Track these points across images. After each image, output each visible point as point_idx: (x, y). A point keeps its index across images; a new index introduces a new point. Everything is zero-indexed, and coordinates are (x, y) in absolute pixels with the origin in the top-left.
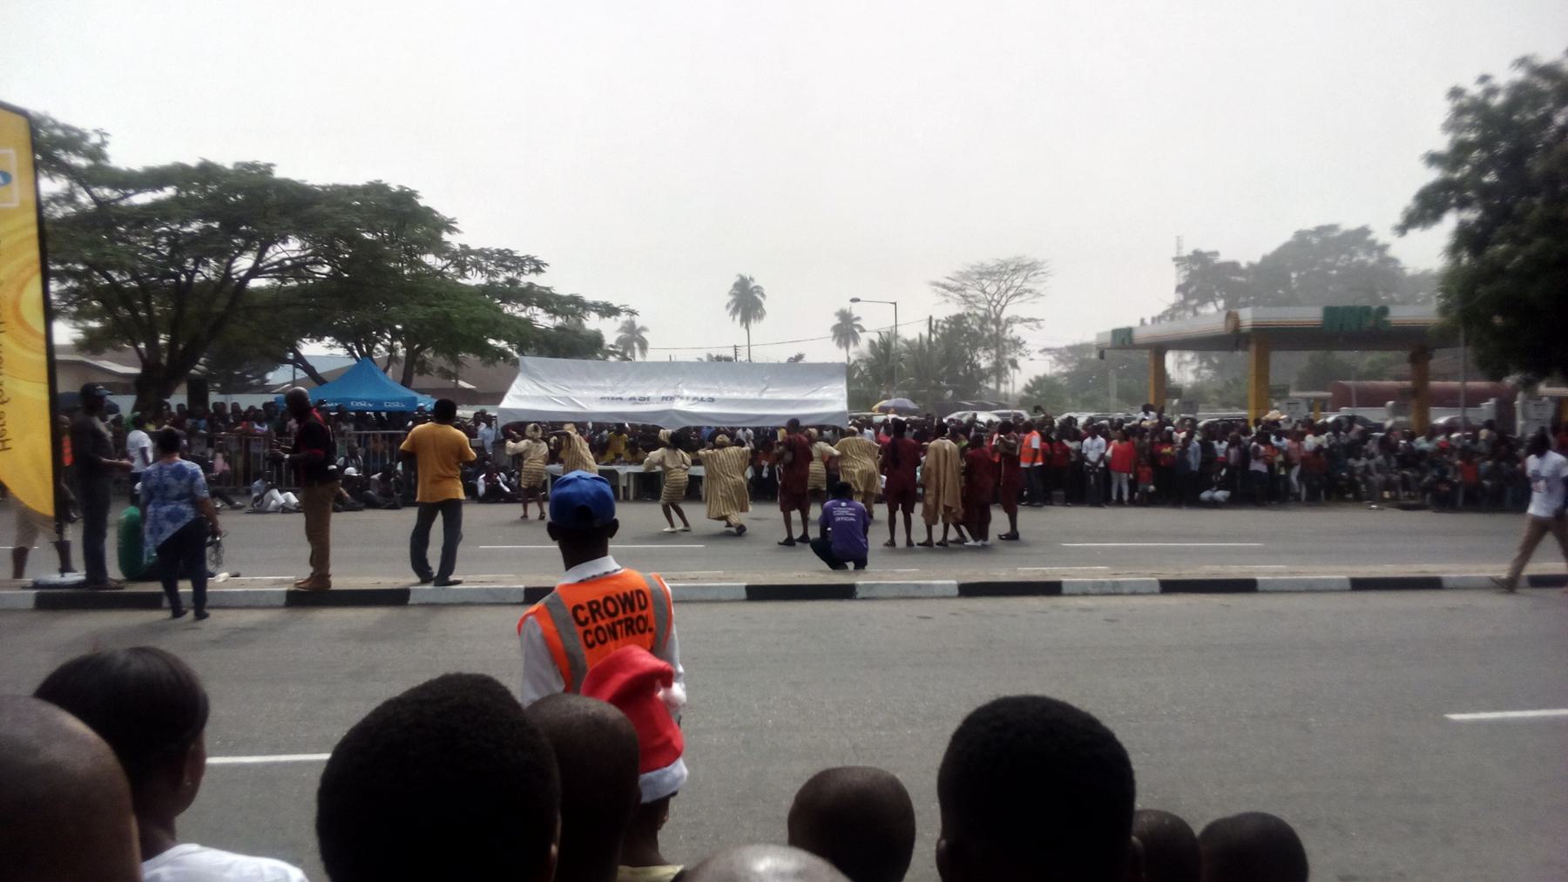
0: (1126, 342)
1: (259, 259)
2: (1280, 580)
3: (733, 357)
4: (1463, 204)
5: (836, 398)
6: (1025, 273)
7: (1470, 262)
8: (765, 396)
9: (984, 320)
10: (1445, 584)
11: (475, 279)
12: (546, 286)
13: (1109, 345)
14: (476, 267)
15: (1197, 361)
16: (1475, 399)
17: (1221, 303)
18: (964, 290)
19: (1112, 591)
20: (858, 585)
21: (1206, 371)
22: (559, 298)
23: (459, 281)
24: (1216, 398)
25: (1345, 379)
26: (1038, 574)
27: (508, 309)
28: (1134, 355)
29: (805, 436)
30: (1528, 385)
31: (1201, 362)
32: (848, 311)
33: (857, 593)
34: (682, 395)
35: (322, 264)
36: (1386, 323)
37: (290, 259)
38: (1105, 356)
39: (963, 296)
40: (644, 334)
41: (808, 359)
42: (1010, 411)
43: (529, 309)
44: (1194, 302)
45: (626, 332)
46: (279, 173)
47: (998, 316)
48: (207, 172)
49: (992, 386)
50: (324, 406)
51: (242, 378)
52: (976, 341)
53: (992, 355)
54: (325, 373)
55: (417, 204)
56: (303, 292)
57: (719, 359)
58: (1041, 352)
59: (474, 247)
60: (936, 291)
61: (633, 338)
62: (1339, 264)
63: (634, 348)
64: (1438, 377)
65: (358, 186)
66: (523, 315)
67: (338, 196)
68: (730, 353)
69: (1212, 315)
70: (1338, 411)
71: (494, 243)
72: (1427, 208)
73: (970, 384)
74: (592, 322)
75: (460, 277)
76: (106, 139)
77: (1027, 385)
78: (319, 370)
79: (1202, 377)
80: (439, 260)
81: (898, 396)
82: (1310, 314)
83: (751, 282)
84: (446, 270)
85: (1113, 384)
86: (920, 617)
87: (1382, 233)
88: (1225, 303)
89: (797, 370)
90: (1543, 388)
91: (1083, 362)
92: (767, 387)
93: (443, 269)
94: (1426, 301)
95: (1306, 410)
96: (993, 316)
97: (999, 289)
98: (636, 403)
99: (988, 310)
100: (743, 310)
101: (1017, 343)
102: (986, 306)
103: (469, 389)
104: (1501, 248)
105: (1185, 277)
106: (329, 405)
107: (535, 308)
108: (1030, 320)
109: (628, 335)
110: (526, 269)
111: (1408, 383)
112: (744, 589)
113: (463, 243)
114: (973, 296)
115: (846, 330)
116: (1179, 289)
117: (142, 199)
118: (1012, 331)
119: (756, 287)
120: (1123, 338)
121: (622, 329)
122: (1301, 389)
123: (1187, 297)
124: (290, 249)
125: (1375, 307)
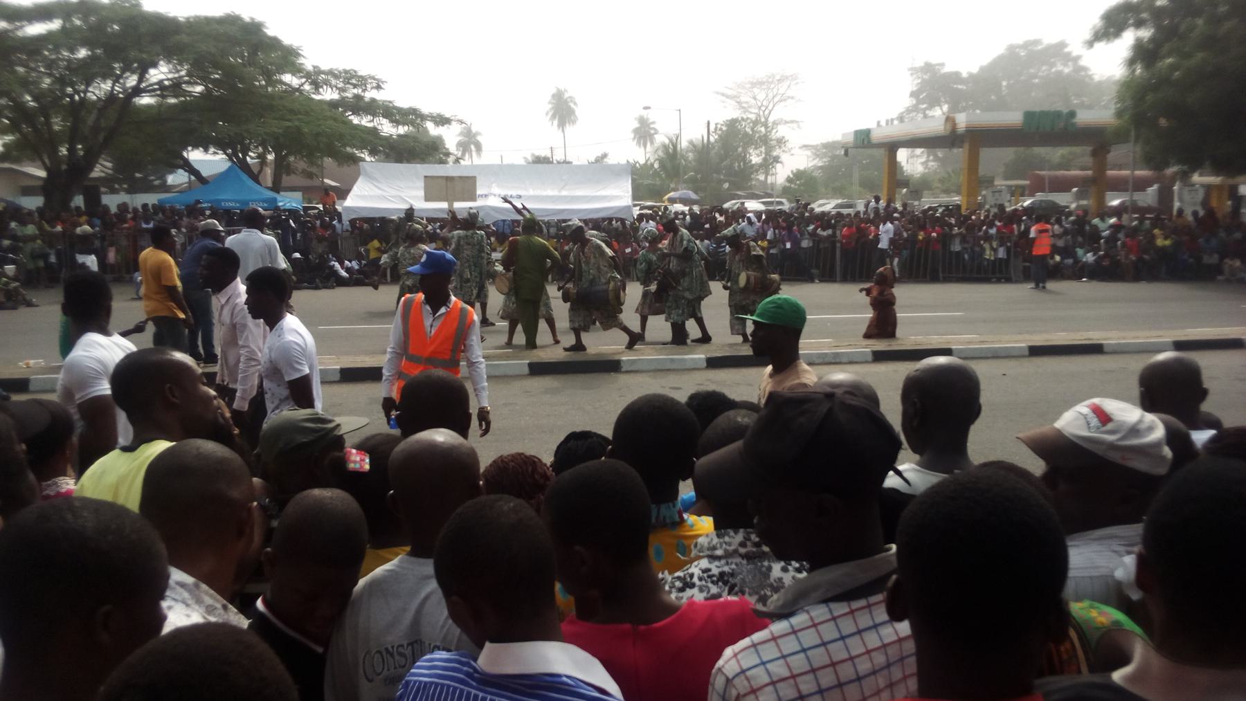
0: (866, 142)
1: (140, 80)
3: (550, 156)
4: (1139, 24)
5: (622, 194)
6: (788, 83)
7: (1141, 73)
8: (564, 193)
9: (756, 123)
10: (1106, 349)
11: (328, 95)
12: (389, 100)
13: (852, 145)
14: (326, 85)
16: (1141, 185)
17: (945, 108)
18: (739, 97)
19: (833, 361)
20: (622, 360)
21: (933, 164)
22: (400, 110)
23: (314, 96)
24: (939, 185)
25: (1040, 170)
27: (355, 120)
30: (1185, 176)
31: (928, 157)
32: (645, 117)
33: (622, 367)
35: (197, 84)
36: (1074, 124)
37: (168, 79)
39: (738, 102)
40: (479, 138)
41: (610, 160)
42: (773, 200)
44: (924, 106)
45: (465, 136)
47: (767, 120)
49: (762, 177)
50: (199, 206)
51: (144, 179)
53: (761, 152)
54: (208, 177)
55: (265, 34)
56: (183, 107)
58: (800, 148)
59: (324, 67)
62: (1040, 74)
63: (471, 151)
65: (216, 17)
69: (935, 120)
70: (1034, 196)
71: (340, 65)
72: (1112, 25)
73: (742, 179)
74: (432, 129)
75: (314, 93)
77: (789, 177)
78: (205, 173)
79: (929, 169)
81: (685, 189)
82: (1013, 118)
84: (302, 88)
85: (856, 177)
86: (671, 388)
87: (1076, 47)
88: (949, 108)
89: (600, 168)
90: (1196, 178)
91: (834, 157)
94: (1106, 107)
95: (1009, 195)
96: (763, 120)
101: (781, 142)
102: (756, 111)
104: (1169, 60)
105: (918, 84)
106: (203, 205)
107: (381, 118)
108: (792, 122)
111: (1090, 173)
112: (527, 365)
113: (315, 65)
114: (747, 103)
115: (644, 133)
116: (913, 94)
117: (36, 29)
119: (570, 97)
120: (863, 139)
121: (461, 134)
122: (1006, 179)
123: (919, 102)
124: (160, 73)
125: (1065, 111)
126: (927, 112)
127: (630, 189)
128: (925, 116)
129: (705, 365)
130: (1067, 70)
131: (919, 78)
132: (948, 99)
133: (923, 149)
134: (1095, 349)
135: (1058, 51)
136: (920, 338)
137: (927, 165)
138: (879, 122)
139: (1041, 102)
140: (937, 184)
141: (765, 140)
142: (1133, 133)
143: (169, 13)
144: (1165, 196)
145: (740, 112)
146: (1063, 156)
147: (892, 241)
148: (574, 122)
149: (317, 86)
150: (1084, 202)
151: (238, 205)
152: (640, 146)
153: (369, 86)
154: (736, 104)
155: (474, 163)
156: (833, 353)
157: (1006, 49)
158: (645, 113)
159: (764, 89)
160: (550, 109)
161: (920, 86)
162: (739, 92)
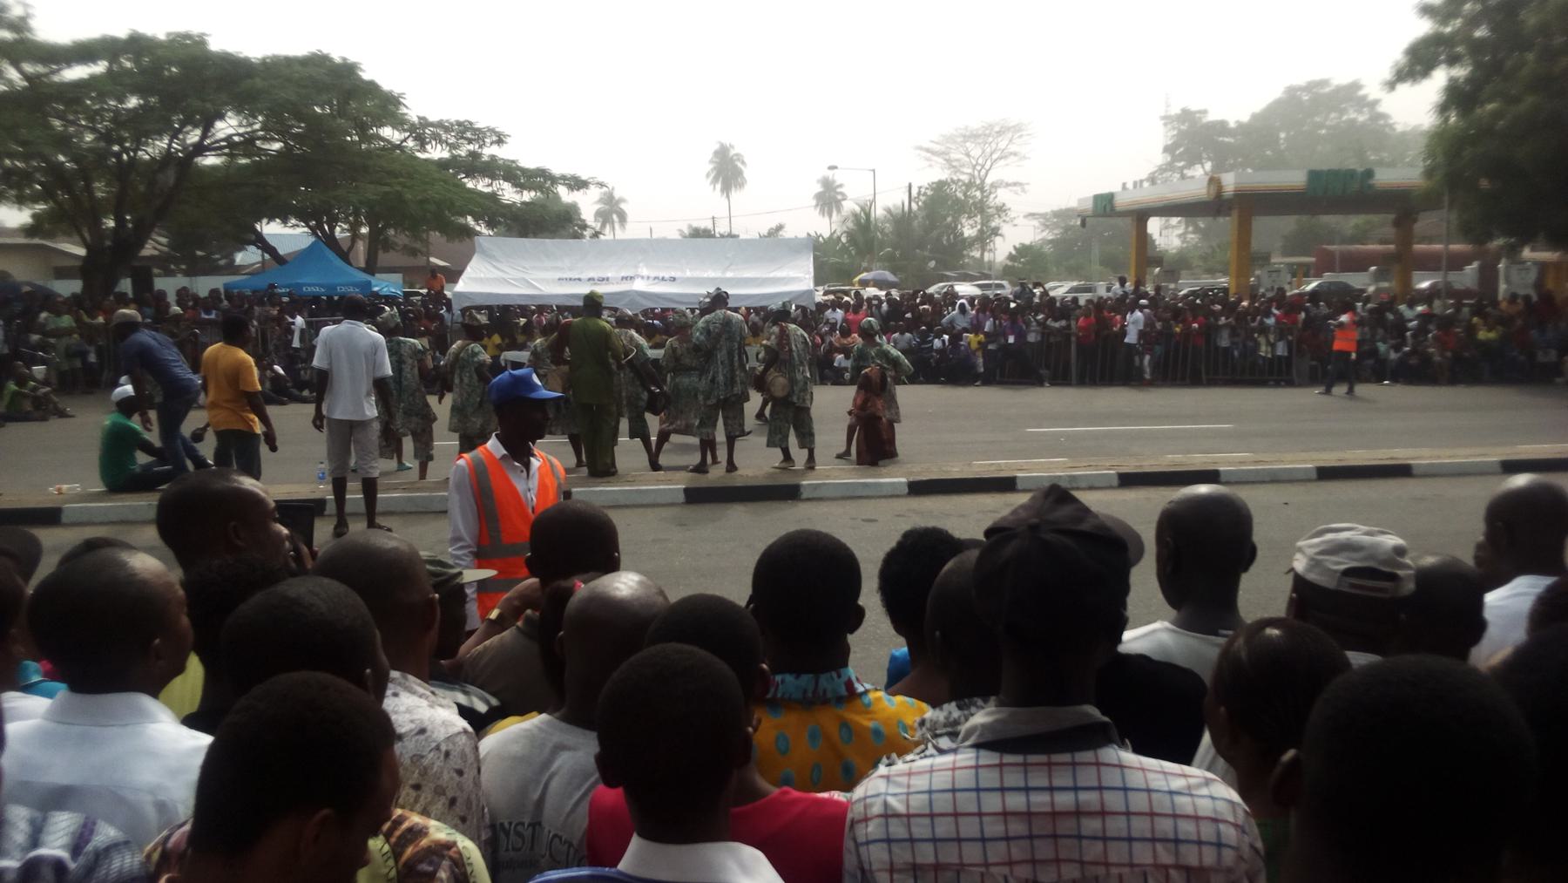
0: (1108, 209)
1: (204, 136)
2: (1243, 470)
4: (1452, 61)
7: (1456, 122)
9: (969, 185)
10: (1415, 472)
11: (436, 152)
13: (1090, 213)
14: (436, 140)
15: (1183, 227)
16: (1457, 263)
17: (1208, 166)
18: (948, 154)
20: (802, 485)
21: (1193, 236)
22: (524, 171)
23: (419, 155)
26: (993, 468)
28: (1119, 221)
29: (765, 323)
30: (1512, 252)
31: (1187, 227)
33: (802, 494)
34: (641, 274)
36: (1371, 186)
38: (1087, 225)
39: (946, 160)
40: (623, 206)
41: (787, 233)
42: (991, 282)
43: (496, 183)
44: (1182, 164)
45: (605, 204)
46: (215, 45)
47: (983, 181)
48: (137, 45)
49: (977, 254)
52: (960, 208)
54: (289, 254)
56: (257, 169)
57: (698, 233)
58: (1026, 217)
59: (433, 118)
60: (919, 155)
61: (612, 210)
62: (1328, 123)
63: (613, 223)
64: (1423, 240)
66: (488, 190)
67: (279, 70)
68: (708, 225)
69: (1195, 181)
70: (1321, 277)
71: (452, 115)
72: (1419, 62)
73: (952, 255)
74: (565, 195)
76: (30, 11)
77: (1010, 253)
78: (77, 238)
79: (1188, 242)
80: (396, 133)
81: (880, 268)
82: (1295, 178)
83: (731, 150)
84: (404, 144)
85: (1096, 252)
86: (863, 520)
87: (1372, 90)
88: (1213, 166)
89: (773, 243)
90: (1527, 253)
91: (1067, 229)
92: (731, 264)
93: (402, 142)
95: (1289, 276)
96: (978, 182)
97: (983, 152)
98: (595, 284)
99: (972, 176)
100: (723, 179)
101: (1001, 210)
102: (970, 171)
103: (443, 267)
104: (1490, 107)
105: (1174, 136)
107: (501, 182)
108: (1015, 184)
109: (607, 207)
110: (488, 140)
111: (1392, 247)
113: (421, 115)
115: (829, 198)
116: (1167, 149)
117: (75, 73)
118: (996, 197)
119: (737, 155)
120: (1105, 204)
121: (600, 201)
123: (1175, 159)
124: (228, 126)
125: (1360, 169)
126: (1185, 171)
127: (812, 270)
128: (1183, 177)
129: (907, 490)
130: (1361, 119)
131: (1174, 129)
132: (1211, 155)
133: (1179, 218)
134: (1401, 471)
135: (1350, 94)
136: (1179, 457)
137: (1185, 238)
138: (1124, 184)
139: (1327, 159)
140: (1196, 262)
141: (981, 208)
142: (1446, 199)
143: (241, 53)
144: (1488, 276)
145: (949, 172)
146: (1356, 226)
147: (1142, 334)
148: (741, 185)
149: (422, 142)
150: (1385, 285)
151: (323, 290)
152: (824, 215)
153: (488, 140)
154: (944, 162)
155: (616, 238)
156: (1070, 476)
157: (1285, 92)
158: (830, 173)
159: (979, 144)
160: (712, 170)
161: (1175, 138)
162: (948, 147)
